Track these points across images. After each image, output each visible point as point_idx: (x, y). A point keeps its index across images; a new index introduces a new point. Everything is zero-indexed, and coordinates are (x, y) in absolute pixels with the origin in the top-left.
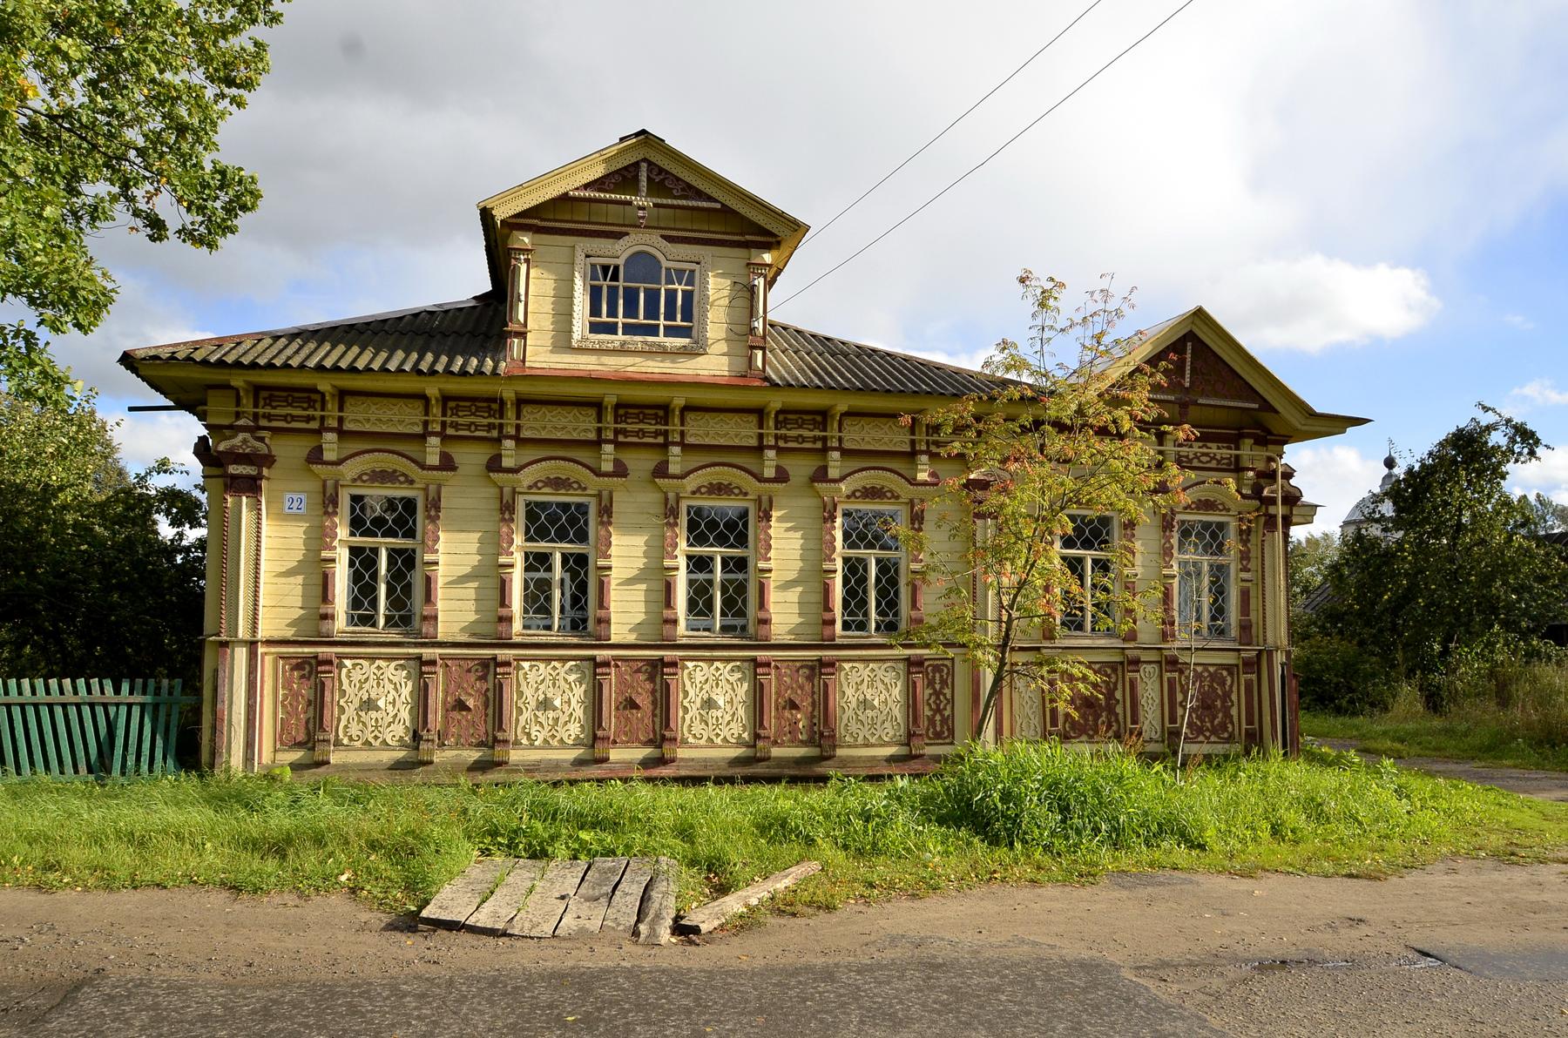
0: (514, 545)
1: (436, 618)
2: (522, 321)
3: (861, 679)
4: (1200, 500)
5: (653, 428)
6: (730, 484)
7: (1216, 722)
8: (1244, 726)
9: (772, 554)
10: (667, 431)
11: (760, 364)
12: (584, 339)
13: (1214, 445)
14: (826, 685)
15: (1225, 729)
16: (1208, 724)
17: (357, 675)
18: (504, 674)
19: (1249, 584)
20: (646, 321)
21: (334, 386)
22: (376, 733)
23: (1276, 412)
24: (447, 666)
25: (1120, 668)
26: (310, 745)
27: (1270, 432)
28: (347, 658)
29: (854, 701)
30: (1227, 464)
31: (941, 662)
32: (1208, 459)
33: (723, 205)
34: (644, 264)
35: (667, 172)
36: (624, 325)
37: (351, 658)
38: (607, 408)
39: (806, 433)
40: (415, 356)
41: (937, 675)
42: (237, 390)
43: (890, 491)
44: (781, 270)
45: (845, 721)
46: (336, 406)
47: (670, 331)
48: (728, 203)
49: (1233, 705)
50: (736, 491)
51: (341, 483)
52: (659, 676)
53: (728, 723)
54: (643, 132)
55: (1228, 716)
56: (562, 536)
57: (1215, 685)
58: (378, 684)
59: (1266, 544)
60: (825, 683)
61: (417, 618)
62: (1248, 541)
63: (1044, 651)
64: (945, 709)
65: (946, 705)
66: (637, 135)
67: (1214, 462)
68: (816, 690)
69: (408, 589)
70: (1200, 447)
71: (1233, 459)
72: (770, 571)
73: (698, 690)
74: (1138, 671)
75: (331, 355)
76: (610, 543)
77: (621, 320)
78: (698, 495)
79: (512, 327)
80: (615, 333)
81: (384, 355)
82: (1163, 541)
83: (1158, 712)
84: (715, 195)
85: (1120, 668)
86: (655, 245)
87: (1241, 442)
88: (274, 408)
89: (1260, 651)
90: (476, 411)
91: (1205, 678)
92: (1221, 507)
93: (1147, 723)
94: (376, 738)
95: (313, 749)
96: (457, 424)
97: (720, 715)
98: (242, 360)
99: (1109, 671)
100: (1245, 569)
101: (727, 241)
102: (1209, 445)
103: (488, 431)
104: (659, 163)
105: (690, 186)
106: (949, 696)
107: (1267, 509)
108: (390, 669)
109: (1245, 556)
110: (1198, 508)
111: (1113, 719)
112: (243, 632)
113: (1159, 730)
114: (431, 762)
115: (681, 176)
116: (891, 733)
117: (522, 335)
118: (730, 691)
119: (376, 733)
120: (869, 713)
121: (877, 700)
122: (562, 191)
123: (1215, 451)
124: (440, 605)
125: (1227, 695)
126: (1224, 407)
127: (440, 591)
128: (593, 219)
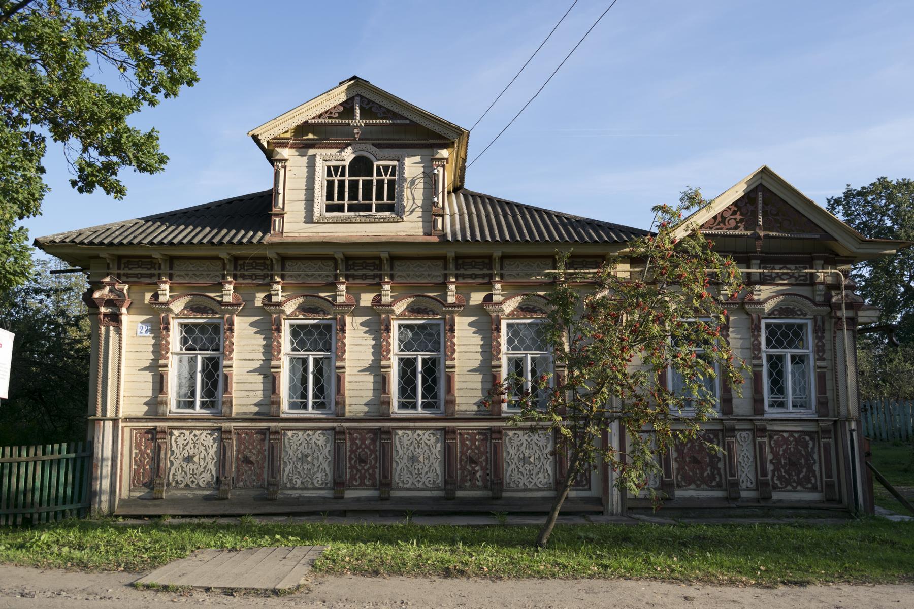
0: (392, 353)
1: (231, 403)
2: (281, 207)
3: (520, 442)
4: (781, 308)
5: (371, 273)
6: (426, 309)
7: (801, 476)
8: (824, 479)
9: (456, 355)
10: (381, 274)
11: (440, 226)
12: (322, 216)
13: (792, 267)
14: (495, 447)
15: (809, 481)
17: (181, 441)
18: (275, 439)
19: (825, 370)
20: (389, 202)
21: (278, 254)
22: (193, 478)
23: (836, 240)
24: (238, 434)
25: (720, 434)
26: (152, 486)
27: (837, 255)
28: (175, 429)
29: (516, 458)
33: (410, 120)
35: (373, 102)
36: (349, 205)
37: (177, 429)
38: (495, 259)
39: (477, 272)
40: (251, 233)
42: (223, 259)
44: (466, 158)
45: (509, 473)
46: (168, 266)
47: (380, 208)
48: (414, 120)
49: (815, 463)
52: (379, 440)
53: (426, 473)
54: (355, 78)
55: (810, 470)
56: (790, 345)
57: (799, 447)
58: (195, 446)
59: (837, 340)
60: (449, 445)
61: (220, 403)
62: (823, 337)
66: (350, 80)
68: (488, 450)
69: (435, 381)
71: (808, 276)
72: (454, 367)
73: (405, 450)
74: (734, 437)
75: (183, 234)
76: (345, 350)
77: (346, 202)
79: (275, 210)
80: (343, 211)
81: (251, 233)
82: (752, 339)
83: (753, 468)
84: (405, 115)
85: (720, 434)
86: (369, 150)
87: (814, 262)
89: (835, 421)
90: (256, 266)
92: (799, 313)
93: (744, 475)
94: (193, 482)
95: (153, 489)
96: (244, 274)
97: (420, 467)
98: (75, 240)
99: (712, 437)
100: (821, 359)
101: (417, 144)
102: (788, 266)
103: (264, 279)
104: (368, 97)
105: (388, 110)
107: (835, 313)
108: (426, 436)
110: (780, 314)
111: (716, 472)
112: (110, 413)
113: (753, 481)
114: (227, 499)
115: (381, 104)
116: (544, 481)
117: (281, 215)
118: (428, 451)
119: (193, 478)
120: (527, 467)
121: (532, 458)
122: (304, 120)
124: (234, 394)
125: (809, 456)
127: (234, 385)
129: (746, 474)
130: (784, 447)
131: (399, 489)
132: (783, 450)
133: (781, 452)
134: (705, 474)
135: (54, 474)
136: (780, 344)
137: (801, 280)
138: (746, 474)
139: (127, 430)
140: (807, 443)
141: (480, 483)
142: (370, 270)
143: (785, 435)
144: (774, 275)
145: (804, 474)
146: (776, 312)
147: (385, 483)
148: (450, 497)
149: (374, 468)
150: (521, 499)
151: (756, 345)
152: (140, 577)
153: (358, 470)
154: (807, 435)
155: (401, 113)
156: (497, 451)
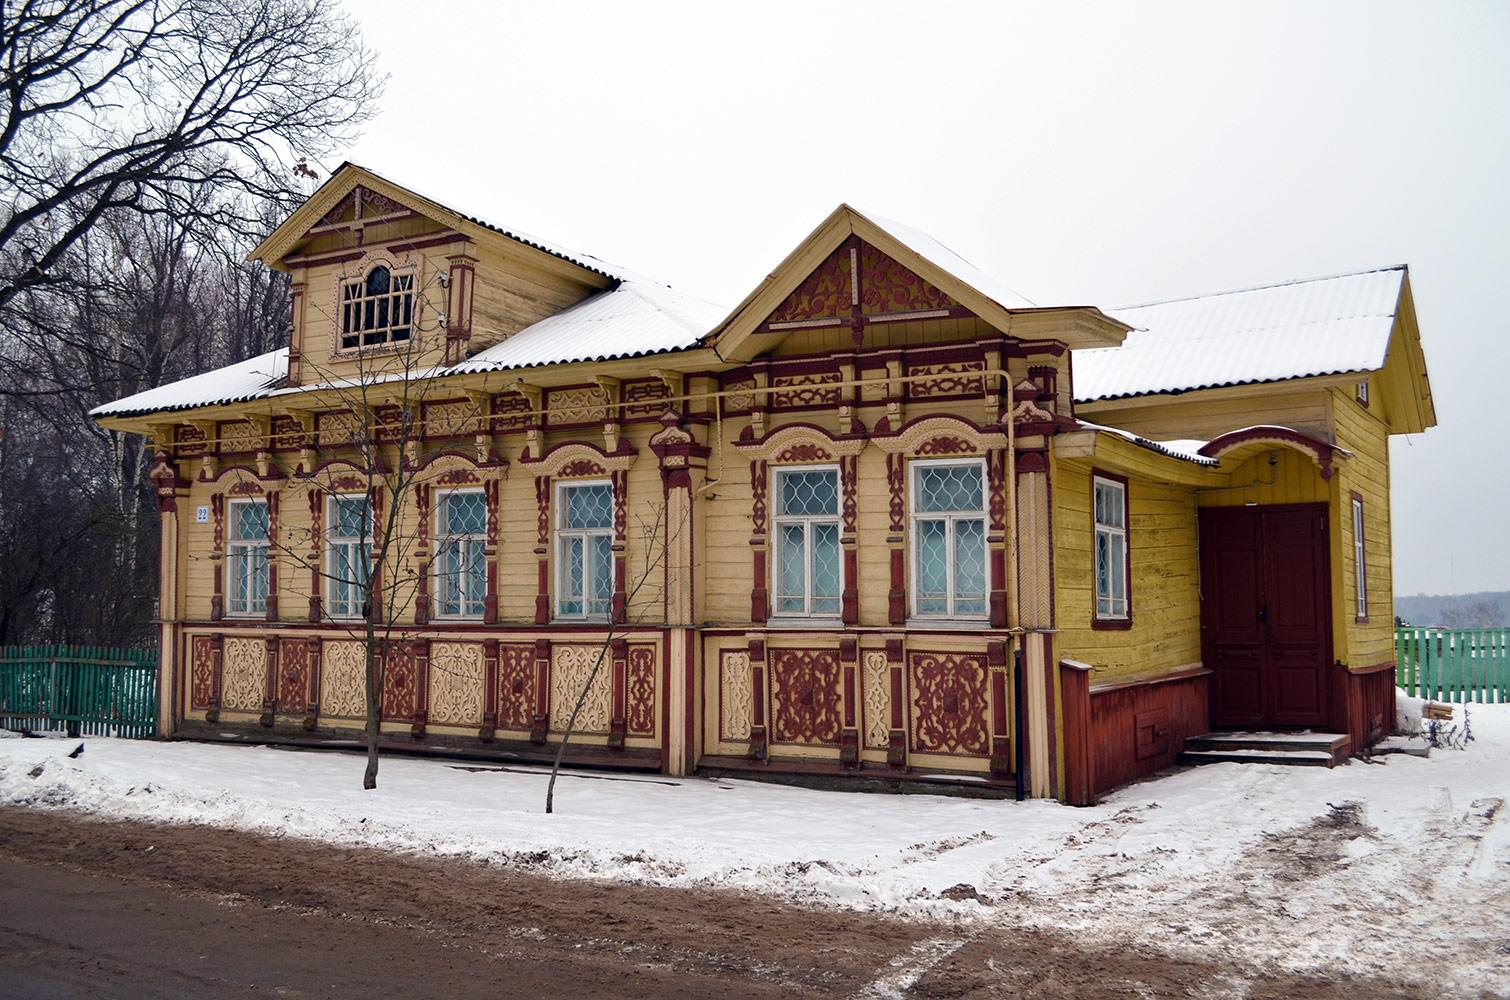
7: (964, 728)
15: (976, 738)
16: (954, 731)
30: (976, 388)
31: (645, 647)
34: (377, 280)
41: (642, 661)
43: (821, 449)
49: (986, 707)
50: (820, 453)
54: (346, 164)
55: (978, 719)
64: (648, 698)
65: (649, 694)
67: (960, 387)
78: (923, 454)
91: (949, 670)
101: (434, 240)
102: (952, 366)
106: (196, 678)
109: (998, 508)
110: (934, 450)
126: (884, 322)
128: (346, 245)
129: (877, 722)
130: (938, 678)
132: (936, 685)
133: (933, 688)
134: (819, 721)
136: (577, 525)
137: (830, 399)
138: (877, 722)
140: (974, 674)
141: (524, 721)
144: (929, 384)
145: (968, 725)
146: (788, 455)
147: (421, 717)
149: (410, 693)
151: (851, 506)
153: (511, 703)
154: (975, 659)
156: (317, 663)
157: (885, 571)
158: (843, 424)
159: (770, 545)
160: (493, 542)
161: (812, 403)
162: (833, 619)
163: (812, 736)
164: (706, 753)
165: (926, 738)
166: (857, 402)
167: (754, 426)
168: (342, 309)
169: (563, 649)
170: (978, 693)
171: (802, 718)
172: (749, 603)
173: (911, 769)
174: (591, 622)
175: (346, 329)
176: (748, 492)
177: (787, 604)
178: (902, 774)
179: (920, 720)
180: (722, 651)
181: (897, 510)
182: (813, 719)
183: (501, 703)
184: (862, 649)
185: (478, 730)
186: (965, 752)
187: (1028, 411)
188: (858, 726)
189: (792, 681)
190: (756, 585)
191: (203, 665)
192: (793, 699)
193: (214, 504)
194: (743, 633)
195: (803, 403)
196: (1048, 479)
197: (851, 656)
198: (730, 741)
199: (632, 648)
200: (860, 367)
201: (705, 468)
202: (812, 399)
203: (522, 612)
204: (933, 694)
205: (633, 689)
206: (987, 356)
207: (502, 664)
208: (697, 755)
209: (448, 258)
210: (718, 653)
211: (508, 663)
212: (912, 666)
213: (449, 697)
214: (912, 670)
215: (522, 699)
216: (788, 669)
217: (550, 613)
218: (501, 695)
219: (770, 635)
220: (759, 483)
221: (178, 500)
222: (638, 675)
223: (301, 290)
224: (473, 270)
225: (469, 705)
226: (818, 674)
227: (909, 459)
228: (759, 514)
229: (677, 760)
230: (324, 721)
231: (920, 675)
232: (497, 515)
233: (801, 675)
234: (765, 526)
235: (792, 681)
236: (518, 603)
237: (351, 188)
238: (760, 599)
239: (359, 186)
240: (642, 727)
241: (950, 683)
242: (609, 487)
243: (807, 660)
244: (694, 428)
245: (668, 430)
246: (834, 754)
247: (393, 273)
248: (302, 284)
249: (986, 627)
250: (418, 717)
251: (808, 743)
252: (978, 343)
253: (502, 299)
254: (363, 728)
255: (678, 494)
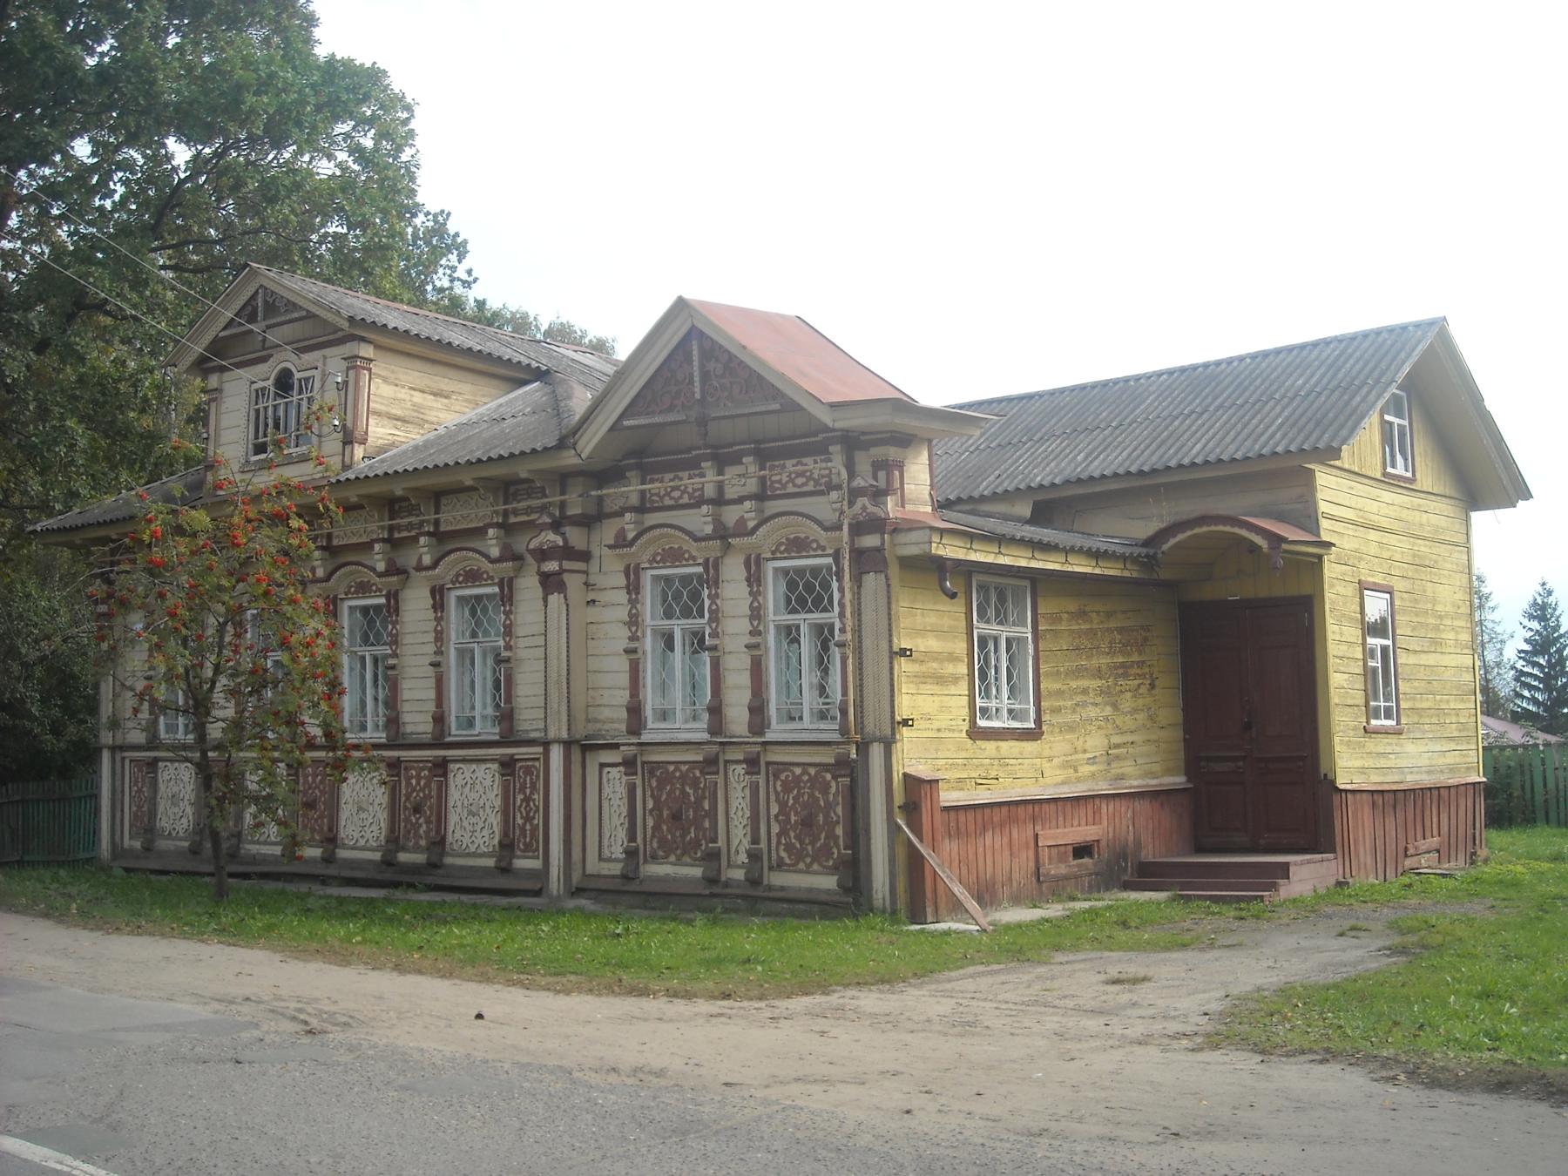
13: (685, 474)
16: (810, 848)
32: (804, 480)
33: (308, 311)
51: (763, 556)
55: (832, 836)
63: (622, 748)
64: (534, 818)
70: (671, 480)
88: (519, 502)
101: (328, 341)
102: (805, 460)
110: (465, 581)
123: (686, 481)
131: (345, 847)
133: (791, 802)
135: (1444, 817)
139: (127, 762)
140: (827, 786)
141: (423, 843)
142: (538, 498)
143: (798, 771)
145: (822, 841)
148: (505, 870)
150: (462, 868)
152: (774, 1093)
154: (827, 771)
155: (300, 304)
157: (745, 679)
158: (705, 523)
159: (644, 652)
160: (508, 647)
161: (681, 502)
162: (698, 731)
163: (811, 863)
164: (588, 872)
165: (783, 854)
166: (720, 501)
167: (626, 527)
168: (252, 413)
169: (458, 766)
170: (830, 806)
171: (673, 836)
172: (624, 714)
173: (770, 888)
174: (483, 738)
175: (256, 437)
176: (622, 597)
177: (664, 715)
178: (759, 892)
179: (779, 835)
180: (602, 766)
181: (756, 614)
182: (683, 836)
183: (402, 824)
184: (726, 762)
185: (280, 848)
186: (821, 869)
187: (864, 508)
188: (721, 843)
189: (664, 797)
190: (631, 696)
191: (139, 791)
192: (665, 816)
193: (434, 597)
194: (616, 746)
195: (672, 502)
196: (887, 579)
197: (713, 769)
198: (610, 860)
199: (519, 765)
200: (722, 462)
201: (586, 572)
202: (681, 497)
203: (421, 728)
204: (791, 808)
205: (520, 807)
206: (831, 449)
207: (403, 784)
208: (576, 877)
209: (345, 359)
210: (597, 768)
211: (409, 784)
212: (771, 778)
213: (356, 818)
214: (771, 783)
215: (422, 820)
216: (660, 787)
217: (446, 728)
218: (402, 817)
219: (644, 748)
220: (633, 588)
221: (566, 577)
222: (525, 794)
223: (215, 394)
224: (370, 370)
225: (374, 828)
226: (687, 789)
227: (768, 560)
228: (634, 621)
229: (555, 879)
230: (248, 847)
231: (779, 789)
232: (512, 617)
233: (672, 791)
234: (639, 634)
235: (664, 797)
236: (417, 721)
237: (254, 290)
238: (635, 711)
239: (261, 286)
240: (528, 847)
241: (806, 797)
242: (829, 568)
243: (678, 774)
244: (568, 530)
245: (543, 534)
246: (697, 872)
247: (297, 375)
248: (216, 390)
249: (705, 736)
250: (146, 831)
251: (679, 862)
252: (694, 453)
253: (408, 397)
254: (279, 853)
255: (555, 599)
